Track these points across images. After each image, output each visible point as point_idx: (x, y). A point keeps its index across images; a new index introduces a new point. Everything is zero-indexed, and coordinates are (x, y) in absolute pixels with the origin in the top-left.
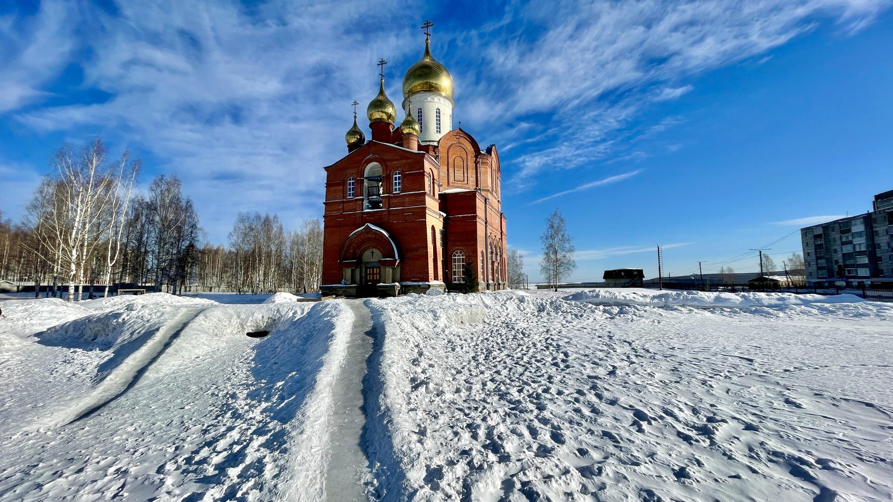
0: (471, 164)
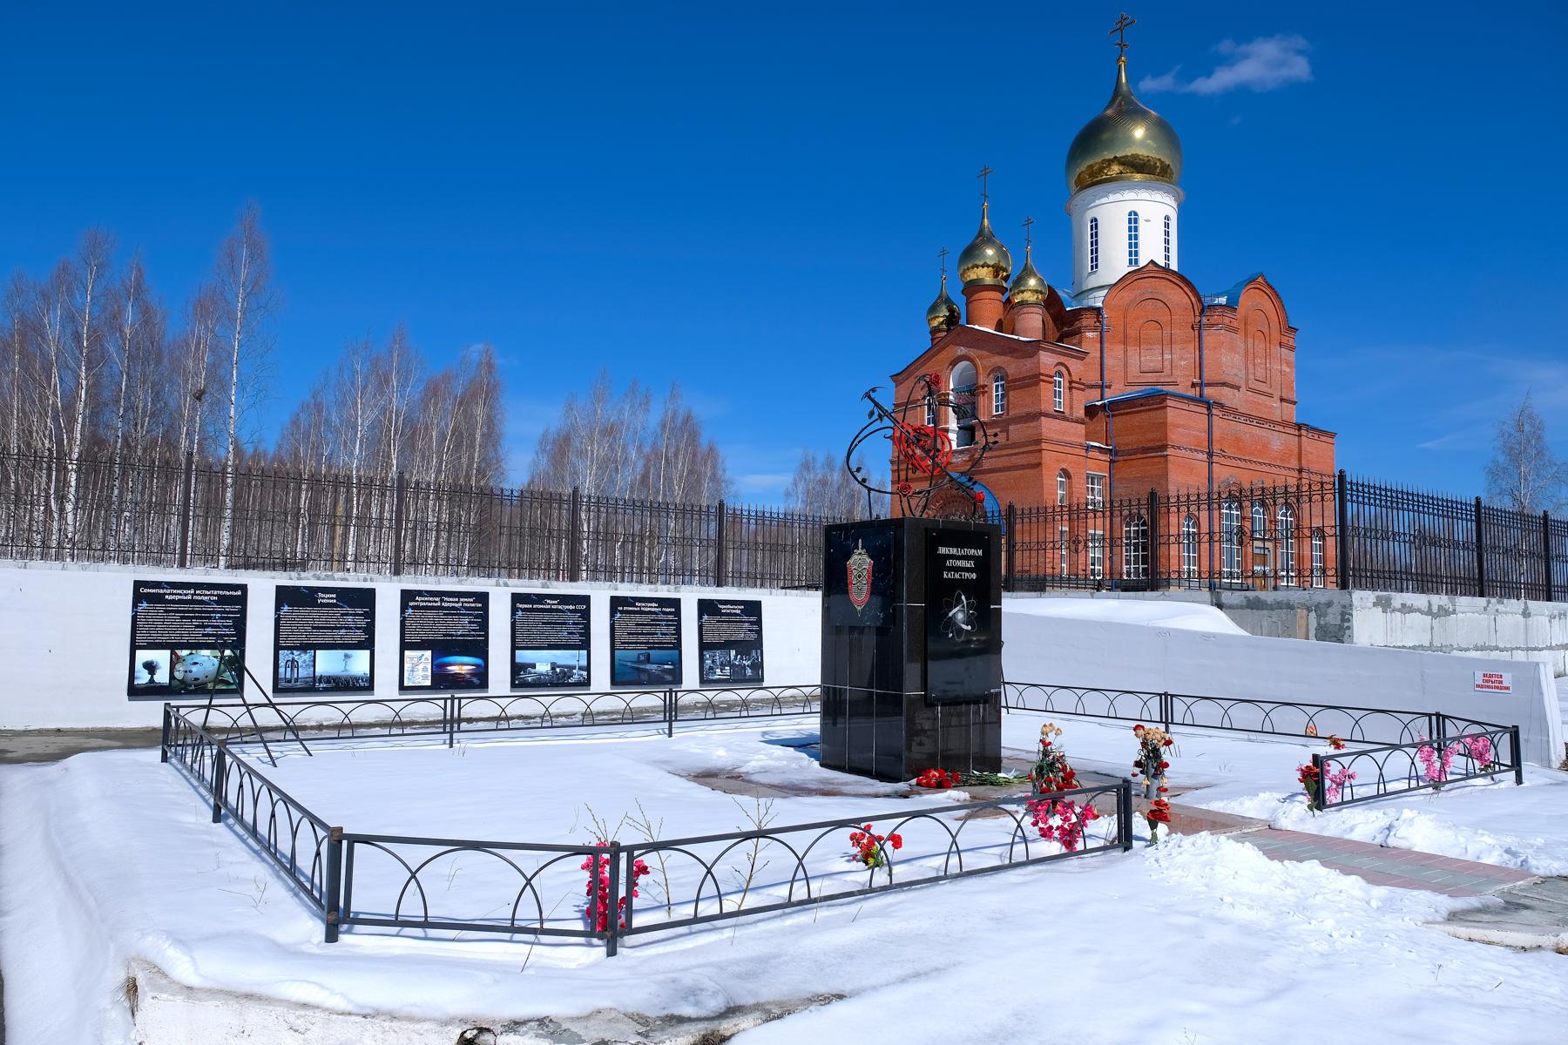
0: (1183, 332)
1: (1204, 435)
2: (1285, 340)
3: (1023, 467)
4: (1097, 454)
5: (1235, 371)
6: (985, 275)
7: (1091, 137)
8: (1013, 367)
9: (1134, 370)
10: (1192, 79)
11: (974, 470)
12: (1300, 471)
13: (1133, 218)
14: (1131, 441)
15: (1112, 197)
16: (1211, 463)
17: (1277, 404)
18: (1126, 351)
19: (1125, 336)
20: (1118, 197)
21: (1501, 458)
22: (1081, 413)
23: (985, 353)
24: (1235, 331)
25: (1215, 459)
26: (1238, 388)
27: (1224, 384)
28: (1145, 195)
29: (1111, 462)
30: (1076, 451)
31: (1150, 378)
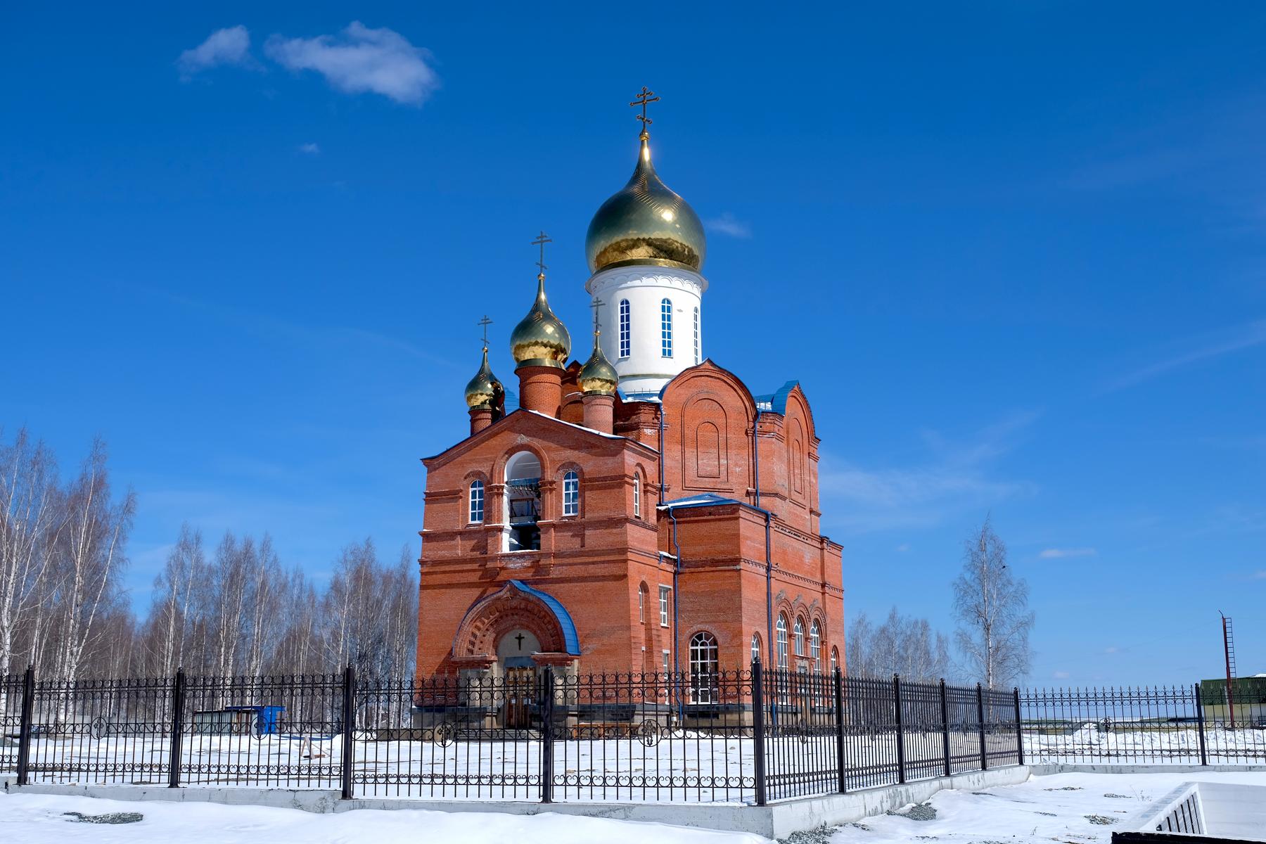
0: (737, 438)
1: (764, 548)
3: (604, 578)
4: (664, 565)
6: (543, 355)
7: (616, 213)
8: (591, 465)
9: (691, 473)
11: (539, 575)
12: (823, 586)
13: (667, 306)
14: (697, 551)
15: (646, 281)
16: (768, 578)
18: (683, 453)
19: (683, 436)
20: (651, 281)
21: (968, 576)
22: (653, 519)
23: (553, 446)
25: (773, 573)
27: (776, 495)
28: (677, 282)
29: (675, 573)
31: (708, 483)
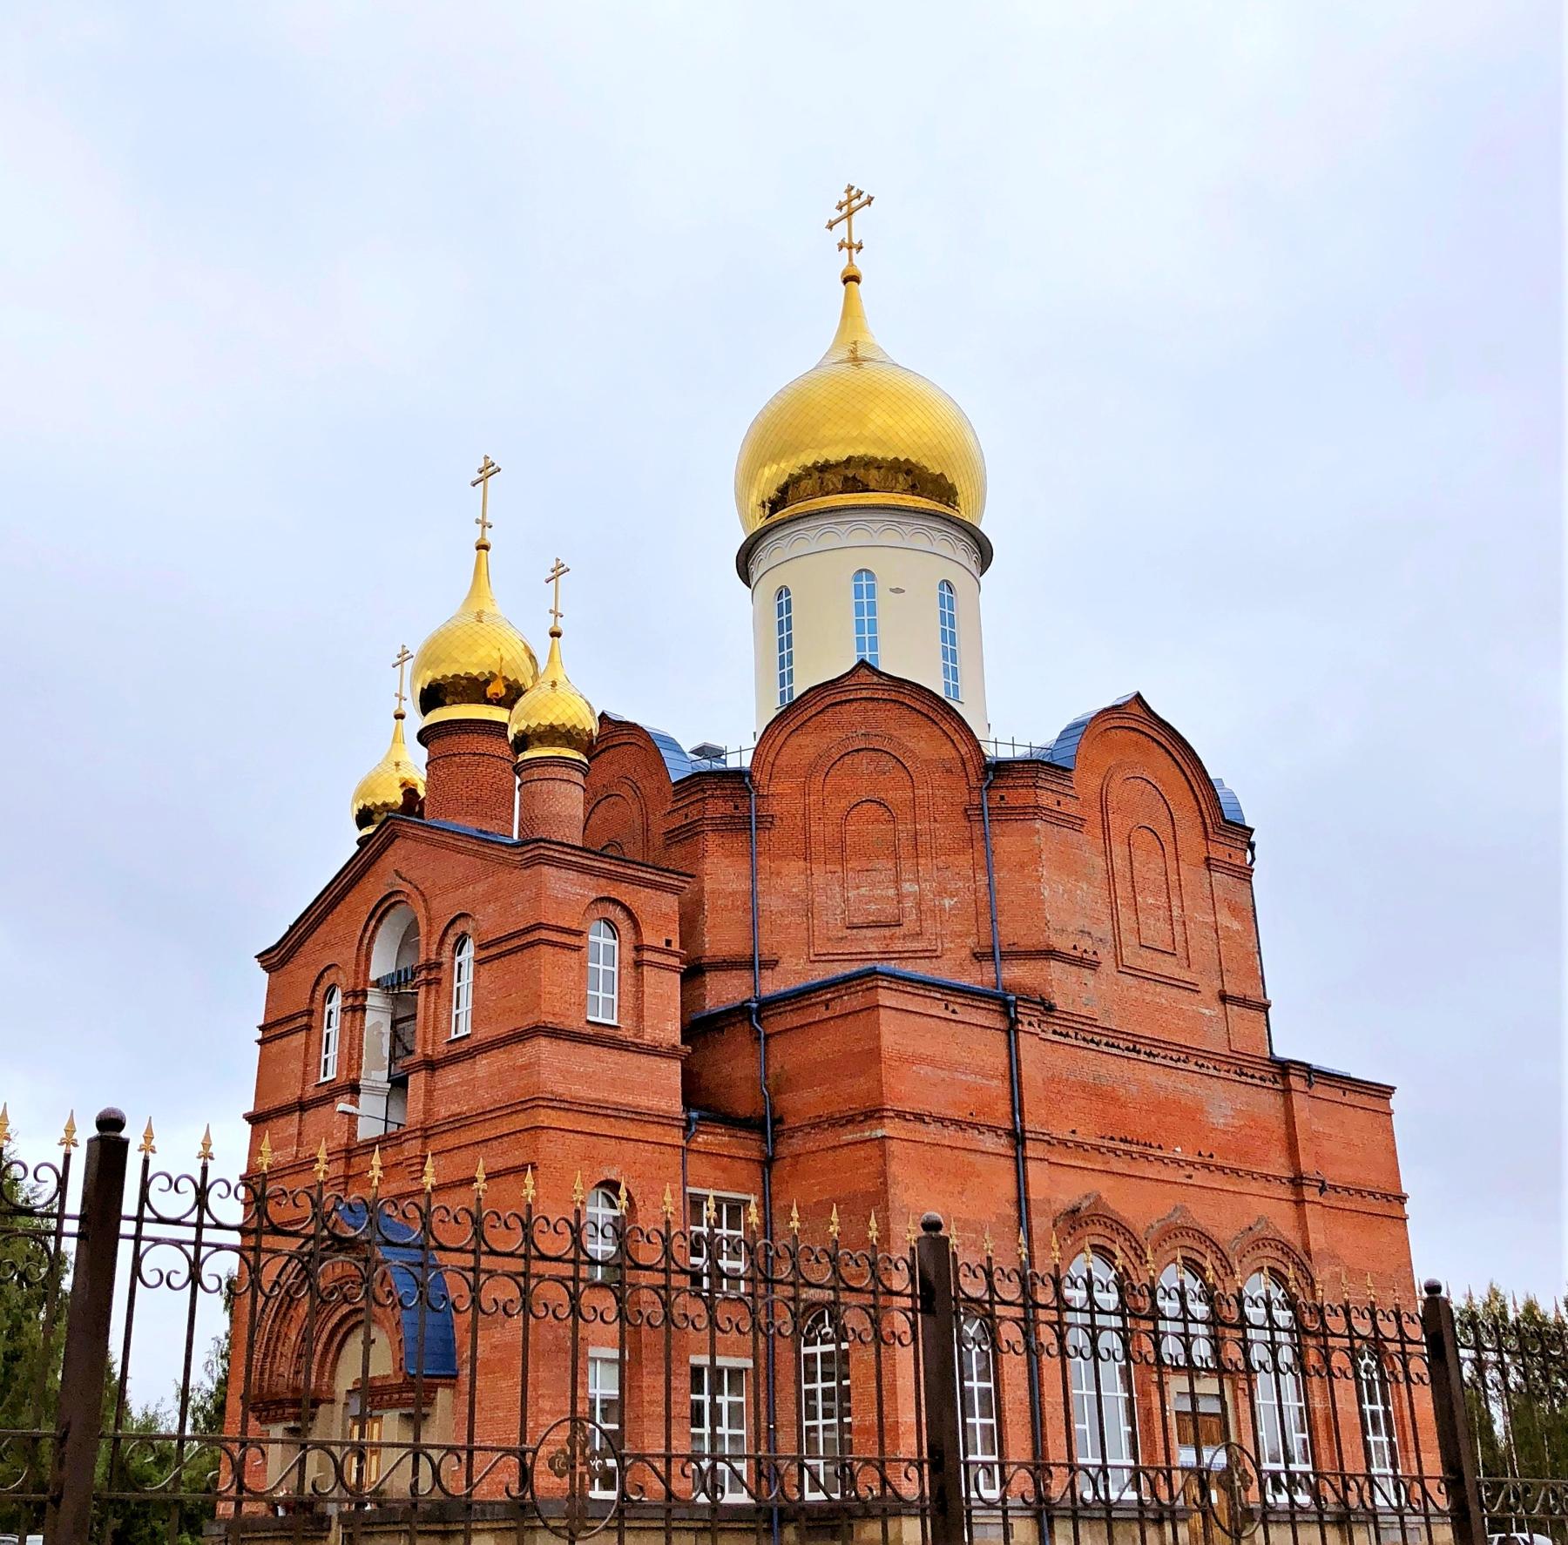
0: (947, 830)
1: (999, 1087)
2: (1219, 852)
5: (1081, 922)
9: (831, 919)
10: (506, 736)
16: (1020, 1161)
17: (1214, 1010)
24: (1075, 823)
25: (1032, 1150)
26: (1094, 966)
30: (654, 1133)
31: (871, 942)
